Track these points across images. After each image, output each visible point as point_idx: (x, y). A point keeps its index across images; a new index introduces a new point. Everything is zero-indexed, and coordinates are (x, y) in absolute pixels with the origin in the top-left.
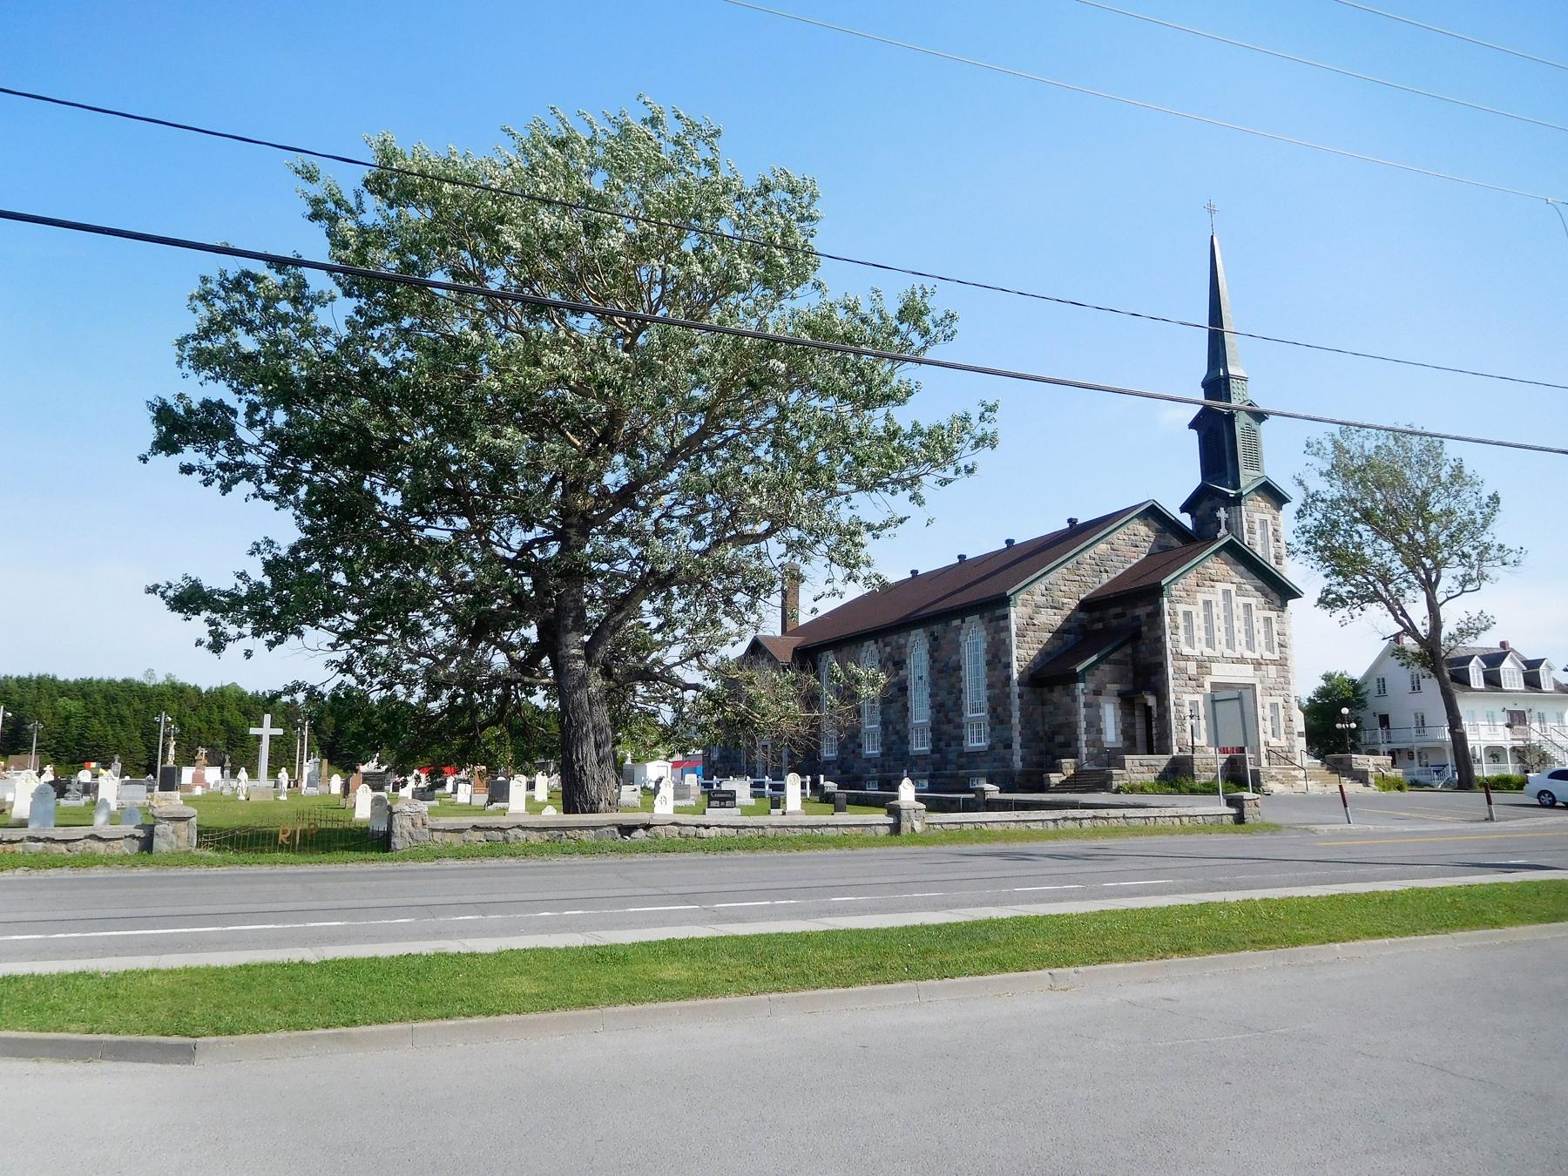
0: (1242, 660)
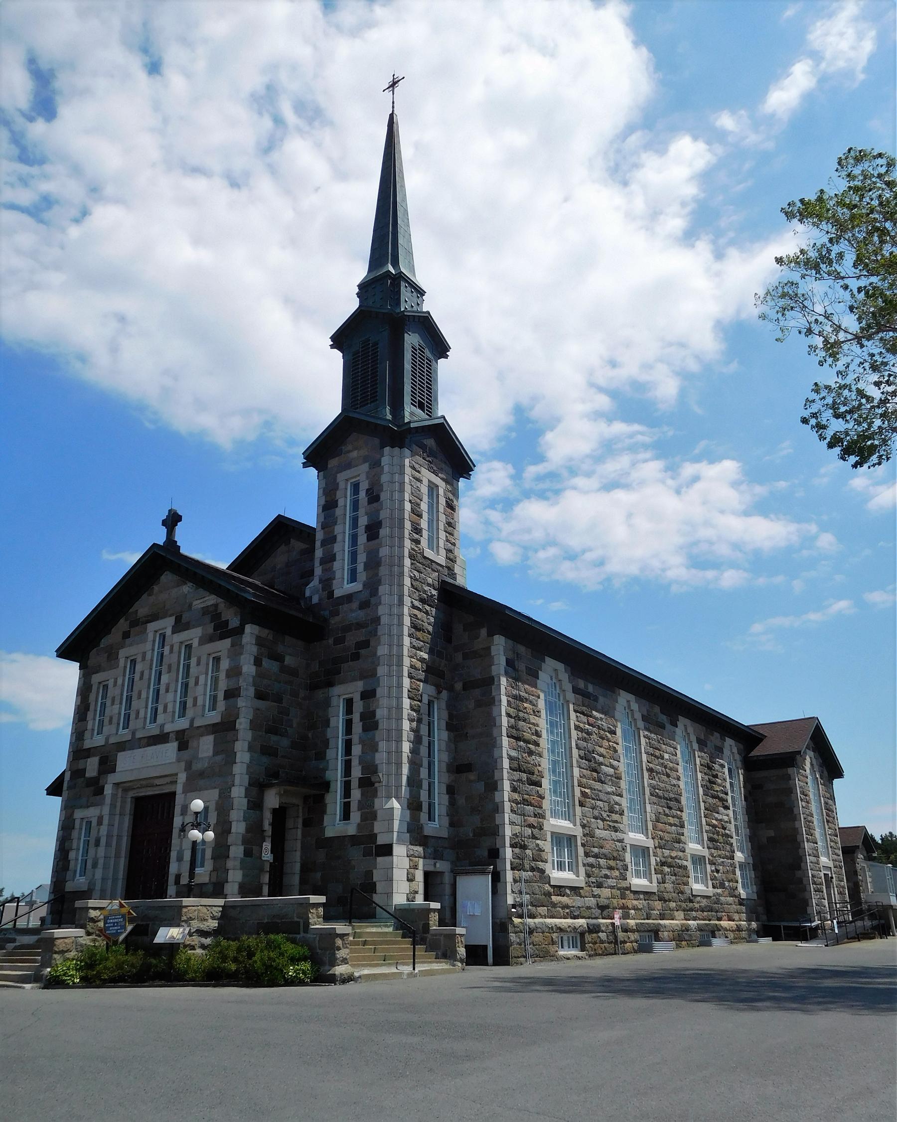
0: (160, 739)
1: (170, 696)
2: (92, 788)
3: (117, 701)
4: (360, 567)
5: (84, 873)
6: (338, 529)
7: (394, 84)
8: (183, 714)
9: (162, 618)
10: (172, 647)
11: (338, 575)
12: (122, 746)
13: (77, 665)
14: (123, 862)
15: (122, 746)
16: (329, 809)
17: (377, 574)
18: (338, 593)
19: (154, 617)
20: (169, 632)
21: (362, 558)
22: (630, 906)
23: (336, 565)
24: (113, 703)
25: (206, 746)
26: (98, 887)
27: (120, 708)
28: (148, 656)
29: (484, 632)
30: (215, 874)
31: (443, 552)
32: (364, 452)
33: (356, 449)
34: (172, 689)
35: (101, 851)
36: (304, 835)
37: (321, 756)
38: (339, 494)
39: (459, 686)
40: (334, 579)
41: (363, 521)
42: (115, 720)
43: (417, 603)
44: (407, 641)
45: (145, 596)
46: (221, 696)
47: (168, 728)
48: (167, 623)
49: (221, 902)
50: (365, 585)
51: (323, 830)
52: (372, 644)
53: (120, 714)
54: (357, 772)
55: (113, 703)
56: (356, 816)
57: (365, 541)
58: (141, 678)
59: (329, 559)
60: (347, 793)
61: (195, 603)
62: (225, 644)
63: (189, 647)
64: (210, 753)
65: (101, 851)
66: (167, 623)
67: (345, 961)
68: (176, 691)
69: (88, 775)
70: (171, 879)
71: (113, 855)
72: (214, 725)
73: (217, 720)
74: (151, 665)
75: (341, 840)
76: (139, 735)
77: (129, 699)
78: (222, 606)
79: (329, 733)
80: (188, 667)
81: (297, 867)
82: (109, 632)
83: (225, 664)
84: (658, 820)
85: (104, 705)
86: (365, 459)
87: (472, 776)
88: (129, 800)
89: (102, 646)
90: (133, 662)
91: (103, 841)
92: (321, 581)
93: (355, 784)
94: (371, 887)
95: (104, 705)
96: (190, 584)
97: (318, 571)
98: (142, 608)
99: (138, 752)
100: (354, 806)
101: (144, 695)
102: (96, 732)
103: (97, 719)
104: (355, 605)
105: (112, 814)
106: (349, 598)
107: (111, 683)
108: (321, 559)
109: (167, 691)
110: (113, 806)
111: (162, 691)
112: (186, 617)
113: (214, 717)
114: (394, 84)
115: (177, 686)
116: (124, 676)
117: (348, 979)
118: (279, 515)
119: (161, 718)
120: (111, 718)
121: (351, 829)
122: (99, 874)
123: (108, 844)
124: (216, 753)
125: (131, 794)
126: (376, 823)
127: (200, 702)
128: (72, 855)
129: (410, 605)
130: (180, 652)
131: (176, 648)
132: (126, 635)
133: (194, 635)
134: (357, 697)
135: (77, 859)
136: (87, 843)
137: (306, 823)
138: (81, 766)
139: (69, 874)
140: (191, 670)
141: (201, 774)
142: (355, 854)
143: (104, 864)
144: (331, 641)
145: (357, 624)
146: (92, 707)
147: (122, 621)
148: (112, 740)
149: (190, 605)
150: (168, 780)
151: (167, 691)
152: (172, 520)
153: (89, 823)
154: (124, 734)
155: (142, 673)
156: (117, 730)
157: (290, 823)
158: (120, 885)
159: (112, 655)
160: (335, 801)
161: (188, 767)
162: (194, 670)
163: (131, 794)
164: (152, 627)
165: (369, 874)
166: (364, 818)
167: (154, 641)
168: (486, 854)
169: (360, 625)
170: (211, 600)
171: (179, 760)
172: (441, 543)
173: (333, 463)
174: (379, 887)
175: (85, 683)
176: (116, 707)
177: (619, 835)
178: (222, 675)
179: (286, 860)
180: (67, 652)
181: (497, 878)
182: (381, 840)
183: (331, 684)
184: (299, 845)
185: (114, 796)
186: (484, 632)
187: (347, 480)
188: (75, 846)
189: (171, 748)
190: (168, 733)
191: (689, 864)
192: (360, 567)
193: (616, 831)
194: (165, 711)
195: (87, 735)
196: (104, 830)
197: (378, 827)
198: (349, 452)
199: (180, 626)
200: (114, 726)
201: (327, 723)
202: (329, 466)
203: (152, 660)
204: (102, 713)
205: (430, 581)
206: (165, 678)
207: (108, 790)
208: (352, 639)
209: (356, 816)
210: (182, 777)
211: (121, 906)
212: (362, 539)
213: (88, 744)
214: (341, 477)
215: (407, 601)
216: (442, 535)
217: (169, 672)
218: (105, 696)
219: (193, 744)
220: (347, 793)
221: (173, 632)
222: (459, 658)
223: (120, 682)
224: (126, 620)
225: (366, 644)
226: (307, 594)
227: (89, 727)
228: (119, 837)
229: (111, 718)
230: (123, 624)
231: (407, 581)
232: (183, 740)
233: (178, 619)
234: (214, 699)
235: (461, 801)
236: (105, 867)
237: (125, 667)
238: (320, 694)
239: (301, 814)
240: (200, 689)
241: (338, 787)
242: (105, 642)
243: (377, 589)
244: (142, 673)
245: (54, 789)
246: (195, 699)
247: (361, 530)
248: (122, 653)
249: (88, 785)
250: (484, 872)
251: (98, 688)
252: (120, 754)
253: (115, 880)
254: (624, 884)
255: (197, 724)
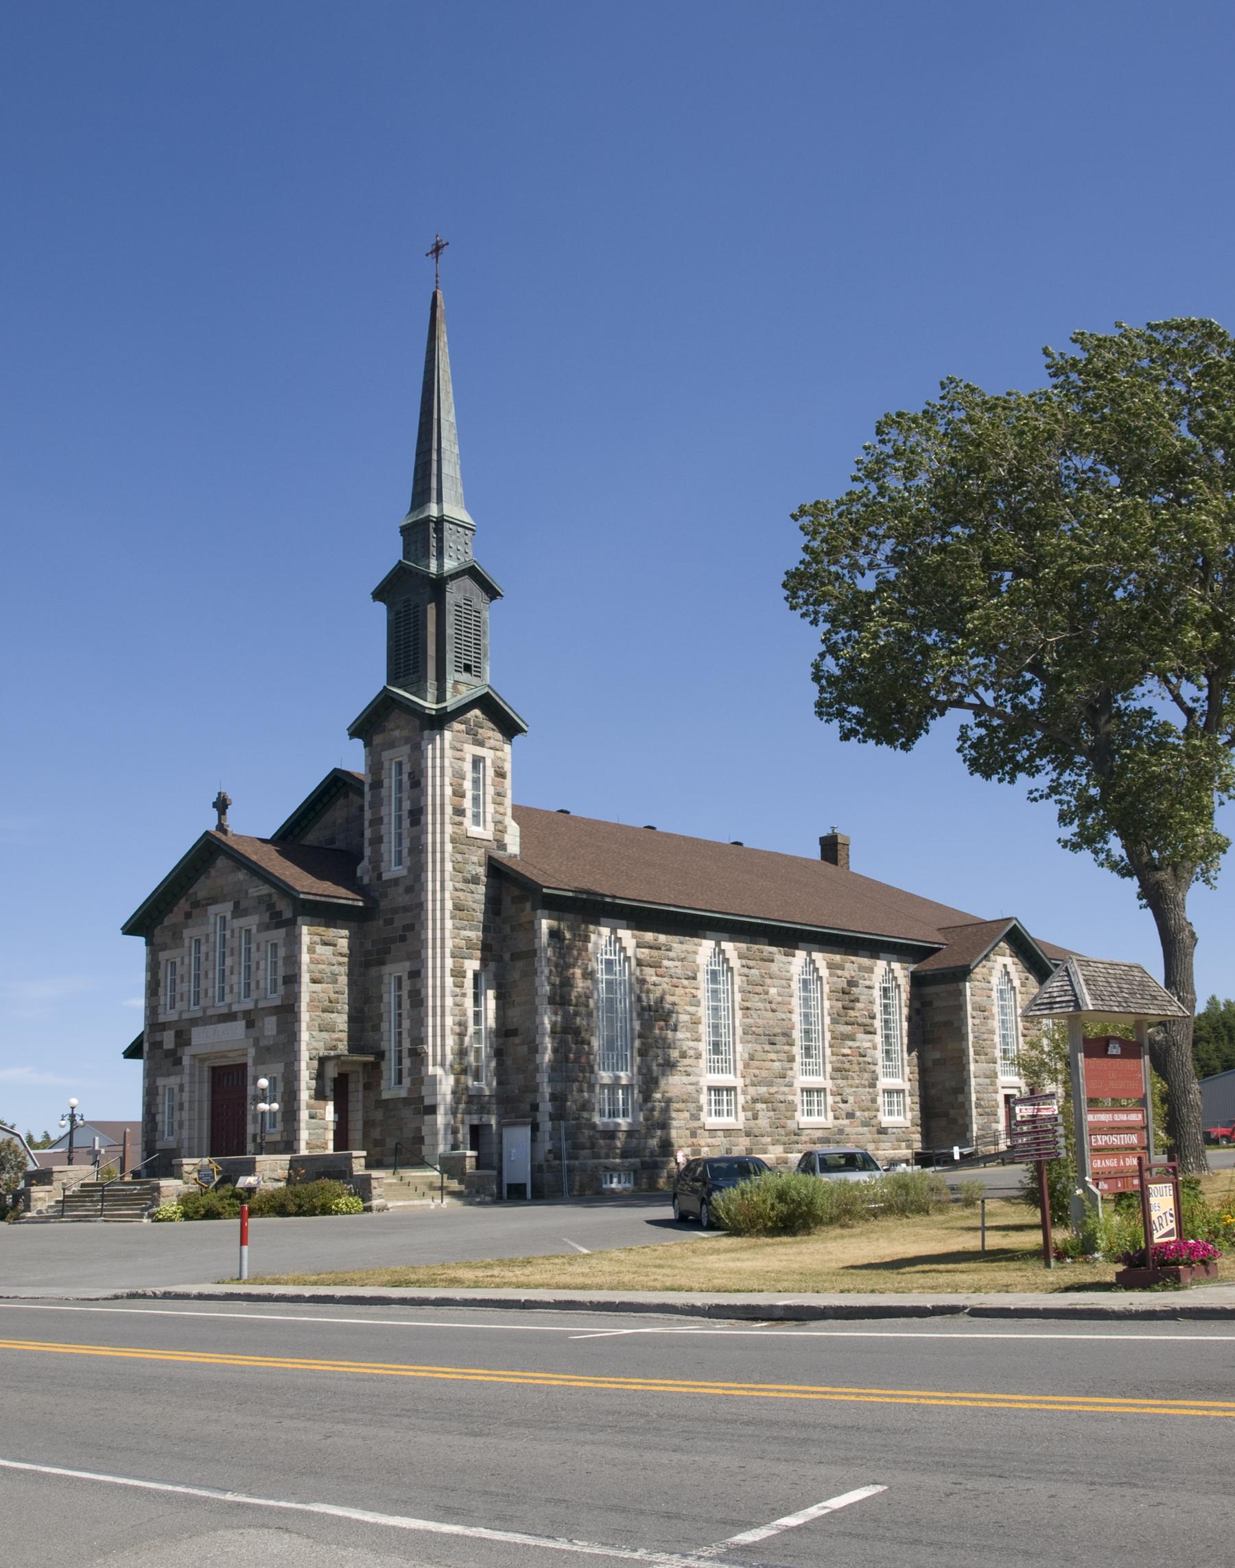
0: (229, 1017)
1: (235, 979)
2: (171, 1059)
3: (186, 979)
4: (405, 852)
5: (171, 1133)
6: (384, 811)
7: (437, 249)
8: (247, 995)
9: (221, 902)
10: (233, 931)
11: (386, 857)
12: (194, 1022)
13: (142, 940)
14: (206, 1124)
15: (194, 1022)
16: (385, 1074)
17: (419, 861)
18: (386, 876)
19: (213, 900)
20: (229, 916)
21: (406, 843)
22: (703, 1144)
23: (384, 847)
24: (182, 981)
25: (270, 1025)
26: (186, 1144)
27: (190, 986)
28: (211, 940)
29: (528, 906)
30: (285, 1134)
31: (491, 826)
32: (405, 733)
33: (398, 727)
34: (236, 971)
35: (185, 1115)
36: (365, 1097)
37: (376, 1028)
38: (384, 774)
39: (507, 957)
40: (382, 861)
41: (407, 805)
42: (185, 998)
43: (459, 886)
44: (449, 924)
45: (203, 878)
46: (280, 981)
47: (235, 1008)
48: (226, 908)
49: (288, 1157)
50: (409, 869)
51: (380, 1094)
52: (417, 927)
53: (189, 991)
54: (406, 1044)
55: (182, 981)
56: (407, 1081)
57: (409, 826)
58: (207, 959)
59: (377, 840)
60: (400, 1062)
61: (250, 891)
62: (282, 932)
63: (248, 931)
64: (274, 1032)
65: (185, 1115)
66: (226, 908)
67: (380, 1196)
68: (240, 973)
69: (165, 1047)
70: (249, 1138)
71: (196, 1117)
72: (276, 1007)
73: (279, 1003)
74: (215, 946)
75: (394, 1100)
76: (210, 1012)
77: (197, 977)
78: (275, 898)
79: (383, 1008)
80: (248, 950)
81: (360, 1125)
82: (171, 911)
83: (282, 952)
84: (752, 1058)
85: (173, 981)
86: (407, 740)
87: (517, 1040)
88: (206, 1069)
89: (165, 924)
90: (198, 941)
91: (186, 1106)
92: (370, 862)
93: (405, 1053)
94: (420, 1140)
95: (173, 981)
96: (245, 871)
97: (367, 851)
98: (201, 889)
99: (210, 1028)
100: (405, 1073)
101: (211, 976)
102: (168, 1007)
103: (169, 994)
104: (401, 889)
105: (191, 1082)
106: (395, 882)
107: (178, 960)
108: (370, 840)
109: (232, 973)
110: (192, 1075)
111: (227, 973)
112: (243, 905)
113: (275, 1000)
114: (437, 249)
115: (240, 968)
116: (190, 955)
117: (383, 1209)
118: (335, 770)
119: (228, 998)
120: (182, 995)
121: (403, 1093)
122: (185, 1133)
123: (191, 1109)
124: (279, 1032)
125: (207, 1064)
126: (423, 1088)
127: (262, 985)
128: (159, 1118)
129: (451, 888)
130: (240, 937)
131: (237, 931)
132: (188, 915)
133: (252, 921)
134: (405, 977)
135: (164, 1122)
136: (172, 1108)
137: (367, 1087)
138: (158, 1039)
139: (158, 1135)
140: (252, 955)
141: (268, 1049)
142: (407, 1113)
143: (190, 1125)
144: (381, 922)
145: (404, 907)
146: (162, 984)
147: (183, 901)
148: (185, 1016)
149: (247, 892)
150: (240, 1053)
151: (232, 973)
152: (222, 805)
153: (171, 1090)
154: (195, 1011)
155: (207, 954)
156: (189, 1007)
157: (351, 1087)
158: (206, 1143)
159: (177, 937)
160: (389, 1069)
161: (256, 1041)
162: (254, 955)
163: (207, 1064)
164: (212, 909)
165: (419, 1129)
166: (413, 1083)
167: (216, 924)
168: (528, 1107)
169: (406, 909)
170: (265, 889)
171: (247, 1037)
172: (489, 818)
173: (378, 739)
174: (427, 1140)
175: (153, 960)
176: (186, 984)
177: (692, 1079)
178: (280, 963)
179: (350, 1119)
180: (132, 928)
181: (535, 1128)
182: (427, 1102)
183: (382, 963)
184: (360, 1106)
185: (192, 1066)
186: (528, 906)
187: (391, 760)
188: (160, 1110)
189: (240, 1025)
190: (236, 1012)
191: (797, 1099)
192: (405, 852)
193: (689, 1075)
194: (231, 991)
195: (161, 1010)
196: (186, 1096)
197: (425, 1091)
198: (392, 730)
199: (238, 912)
200: (185, 1003)
201: (380, 998)
202: (374, 743)
203: (215, 942)
204: (173, 989)
205: (475, 859)
206: (228, 961)
207: (186, 1061)
208: (400, 921)
209: (407, 1081)
210: (252, 1052)
211: (210, 1162)
212: (406, 823)
213: (162, 1019)
214: (386, 755)
215: (449, 885)
216: (490, 808)
217: (232, 955)
218: (173, 973)
219: (258, 1024)
220: (400, 1062)
221: (233, 918)
222: (507, 929)
223: (186, 960)
224: (187, 901)
225: (410, 927)
226: (359, 873)
227: (162, 1002)
228: (200, 1101)
229: (182, 995)
230: (183, 905)
231: (449, 866)
232: (251, 1020)
233: (237, 905)
234: (274, 981)
235: (509, 1062)
236: (191, 1128)
237: (190, 947)
238: (373, 971)
239: (361, 1079)
240: (261, 973)
241: (392, 1056)
242: (168, 921)
243: (420, 875)
244: (207, 954)
245: (133, 1052)
246: (258, 982)
247: (405, 814)
248: (186, 933)
249: (166, 1057)
250: (524, 1124)
251: (166, 965)
252: (193, 1029)
253: (200, 1138)
254: (696, 1124)
255: (261, 1005)
